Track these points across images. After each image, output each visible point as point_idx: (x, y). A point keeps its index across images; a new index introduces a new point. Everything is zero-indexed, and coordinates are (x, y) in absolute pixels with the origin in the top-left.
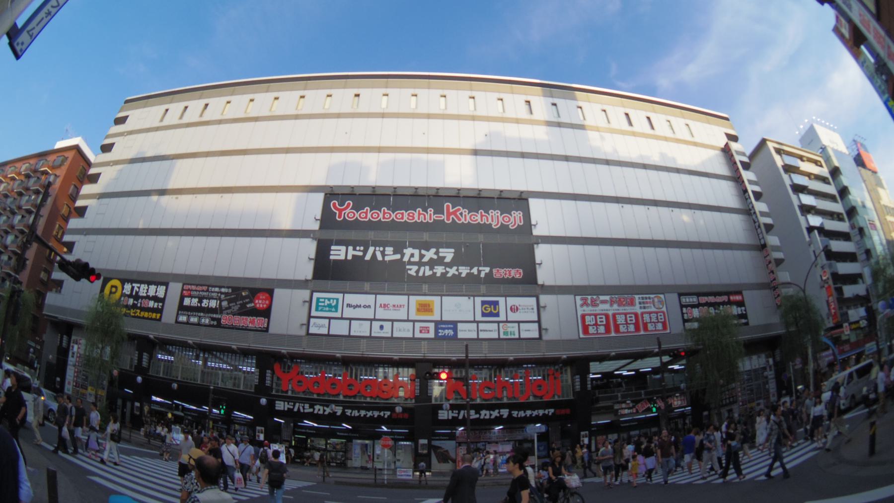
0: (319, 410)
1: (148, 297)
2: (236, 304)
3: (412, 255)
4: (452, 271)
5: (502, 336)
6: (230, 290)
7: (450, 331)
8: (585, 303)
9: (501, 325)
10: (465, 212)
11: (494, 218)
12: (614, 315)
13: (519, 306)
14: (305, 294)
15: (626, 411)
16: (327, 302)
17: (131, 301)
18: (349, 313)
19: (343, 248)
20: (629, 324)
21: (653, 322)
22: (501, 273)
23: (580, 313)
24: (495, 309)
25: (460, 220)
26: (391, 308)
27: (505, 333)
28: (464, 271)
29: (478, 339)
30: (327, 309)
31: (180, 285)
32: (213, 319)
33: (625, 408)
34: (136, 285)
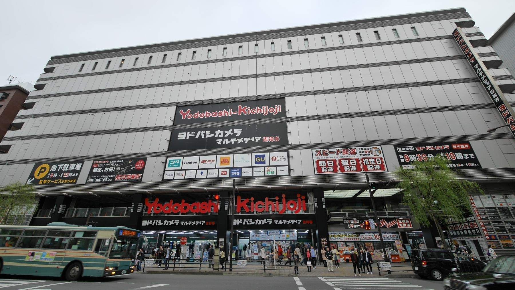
0: (166, 223)
1: (69, 171)
2: (125, 168)
3: (220, 134)
4: (240, 141)
5: (266, 175)
6: (122, 161)
7: (237, 172)
8: (319, 154)
9: (266, 168)
10: (249, 108)
11: (265, 110)
12: (340, 161)
13: (277, 157)
14: (163, 159)
15: (355, 226)
16: (174, 162)
17: (55, 175)
18: (185, 167)
19: (185, 133)
20: (352, 166)
21: (372, 164)
22: (266, 140)
23: (315, 159)
24: (263, 159)
25: (246, 113)
26: (207, 162)
27: (269, 173)
28: (247, 140)
29: (253, 177)
30: (174, 165)
31: (92, 161)
32: (110, 178)
33: (353, 224)
34: (60, 165)
